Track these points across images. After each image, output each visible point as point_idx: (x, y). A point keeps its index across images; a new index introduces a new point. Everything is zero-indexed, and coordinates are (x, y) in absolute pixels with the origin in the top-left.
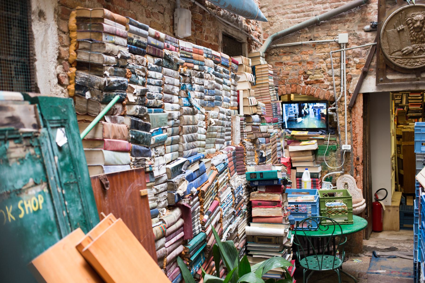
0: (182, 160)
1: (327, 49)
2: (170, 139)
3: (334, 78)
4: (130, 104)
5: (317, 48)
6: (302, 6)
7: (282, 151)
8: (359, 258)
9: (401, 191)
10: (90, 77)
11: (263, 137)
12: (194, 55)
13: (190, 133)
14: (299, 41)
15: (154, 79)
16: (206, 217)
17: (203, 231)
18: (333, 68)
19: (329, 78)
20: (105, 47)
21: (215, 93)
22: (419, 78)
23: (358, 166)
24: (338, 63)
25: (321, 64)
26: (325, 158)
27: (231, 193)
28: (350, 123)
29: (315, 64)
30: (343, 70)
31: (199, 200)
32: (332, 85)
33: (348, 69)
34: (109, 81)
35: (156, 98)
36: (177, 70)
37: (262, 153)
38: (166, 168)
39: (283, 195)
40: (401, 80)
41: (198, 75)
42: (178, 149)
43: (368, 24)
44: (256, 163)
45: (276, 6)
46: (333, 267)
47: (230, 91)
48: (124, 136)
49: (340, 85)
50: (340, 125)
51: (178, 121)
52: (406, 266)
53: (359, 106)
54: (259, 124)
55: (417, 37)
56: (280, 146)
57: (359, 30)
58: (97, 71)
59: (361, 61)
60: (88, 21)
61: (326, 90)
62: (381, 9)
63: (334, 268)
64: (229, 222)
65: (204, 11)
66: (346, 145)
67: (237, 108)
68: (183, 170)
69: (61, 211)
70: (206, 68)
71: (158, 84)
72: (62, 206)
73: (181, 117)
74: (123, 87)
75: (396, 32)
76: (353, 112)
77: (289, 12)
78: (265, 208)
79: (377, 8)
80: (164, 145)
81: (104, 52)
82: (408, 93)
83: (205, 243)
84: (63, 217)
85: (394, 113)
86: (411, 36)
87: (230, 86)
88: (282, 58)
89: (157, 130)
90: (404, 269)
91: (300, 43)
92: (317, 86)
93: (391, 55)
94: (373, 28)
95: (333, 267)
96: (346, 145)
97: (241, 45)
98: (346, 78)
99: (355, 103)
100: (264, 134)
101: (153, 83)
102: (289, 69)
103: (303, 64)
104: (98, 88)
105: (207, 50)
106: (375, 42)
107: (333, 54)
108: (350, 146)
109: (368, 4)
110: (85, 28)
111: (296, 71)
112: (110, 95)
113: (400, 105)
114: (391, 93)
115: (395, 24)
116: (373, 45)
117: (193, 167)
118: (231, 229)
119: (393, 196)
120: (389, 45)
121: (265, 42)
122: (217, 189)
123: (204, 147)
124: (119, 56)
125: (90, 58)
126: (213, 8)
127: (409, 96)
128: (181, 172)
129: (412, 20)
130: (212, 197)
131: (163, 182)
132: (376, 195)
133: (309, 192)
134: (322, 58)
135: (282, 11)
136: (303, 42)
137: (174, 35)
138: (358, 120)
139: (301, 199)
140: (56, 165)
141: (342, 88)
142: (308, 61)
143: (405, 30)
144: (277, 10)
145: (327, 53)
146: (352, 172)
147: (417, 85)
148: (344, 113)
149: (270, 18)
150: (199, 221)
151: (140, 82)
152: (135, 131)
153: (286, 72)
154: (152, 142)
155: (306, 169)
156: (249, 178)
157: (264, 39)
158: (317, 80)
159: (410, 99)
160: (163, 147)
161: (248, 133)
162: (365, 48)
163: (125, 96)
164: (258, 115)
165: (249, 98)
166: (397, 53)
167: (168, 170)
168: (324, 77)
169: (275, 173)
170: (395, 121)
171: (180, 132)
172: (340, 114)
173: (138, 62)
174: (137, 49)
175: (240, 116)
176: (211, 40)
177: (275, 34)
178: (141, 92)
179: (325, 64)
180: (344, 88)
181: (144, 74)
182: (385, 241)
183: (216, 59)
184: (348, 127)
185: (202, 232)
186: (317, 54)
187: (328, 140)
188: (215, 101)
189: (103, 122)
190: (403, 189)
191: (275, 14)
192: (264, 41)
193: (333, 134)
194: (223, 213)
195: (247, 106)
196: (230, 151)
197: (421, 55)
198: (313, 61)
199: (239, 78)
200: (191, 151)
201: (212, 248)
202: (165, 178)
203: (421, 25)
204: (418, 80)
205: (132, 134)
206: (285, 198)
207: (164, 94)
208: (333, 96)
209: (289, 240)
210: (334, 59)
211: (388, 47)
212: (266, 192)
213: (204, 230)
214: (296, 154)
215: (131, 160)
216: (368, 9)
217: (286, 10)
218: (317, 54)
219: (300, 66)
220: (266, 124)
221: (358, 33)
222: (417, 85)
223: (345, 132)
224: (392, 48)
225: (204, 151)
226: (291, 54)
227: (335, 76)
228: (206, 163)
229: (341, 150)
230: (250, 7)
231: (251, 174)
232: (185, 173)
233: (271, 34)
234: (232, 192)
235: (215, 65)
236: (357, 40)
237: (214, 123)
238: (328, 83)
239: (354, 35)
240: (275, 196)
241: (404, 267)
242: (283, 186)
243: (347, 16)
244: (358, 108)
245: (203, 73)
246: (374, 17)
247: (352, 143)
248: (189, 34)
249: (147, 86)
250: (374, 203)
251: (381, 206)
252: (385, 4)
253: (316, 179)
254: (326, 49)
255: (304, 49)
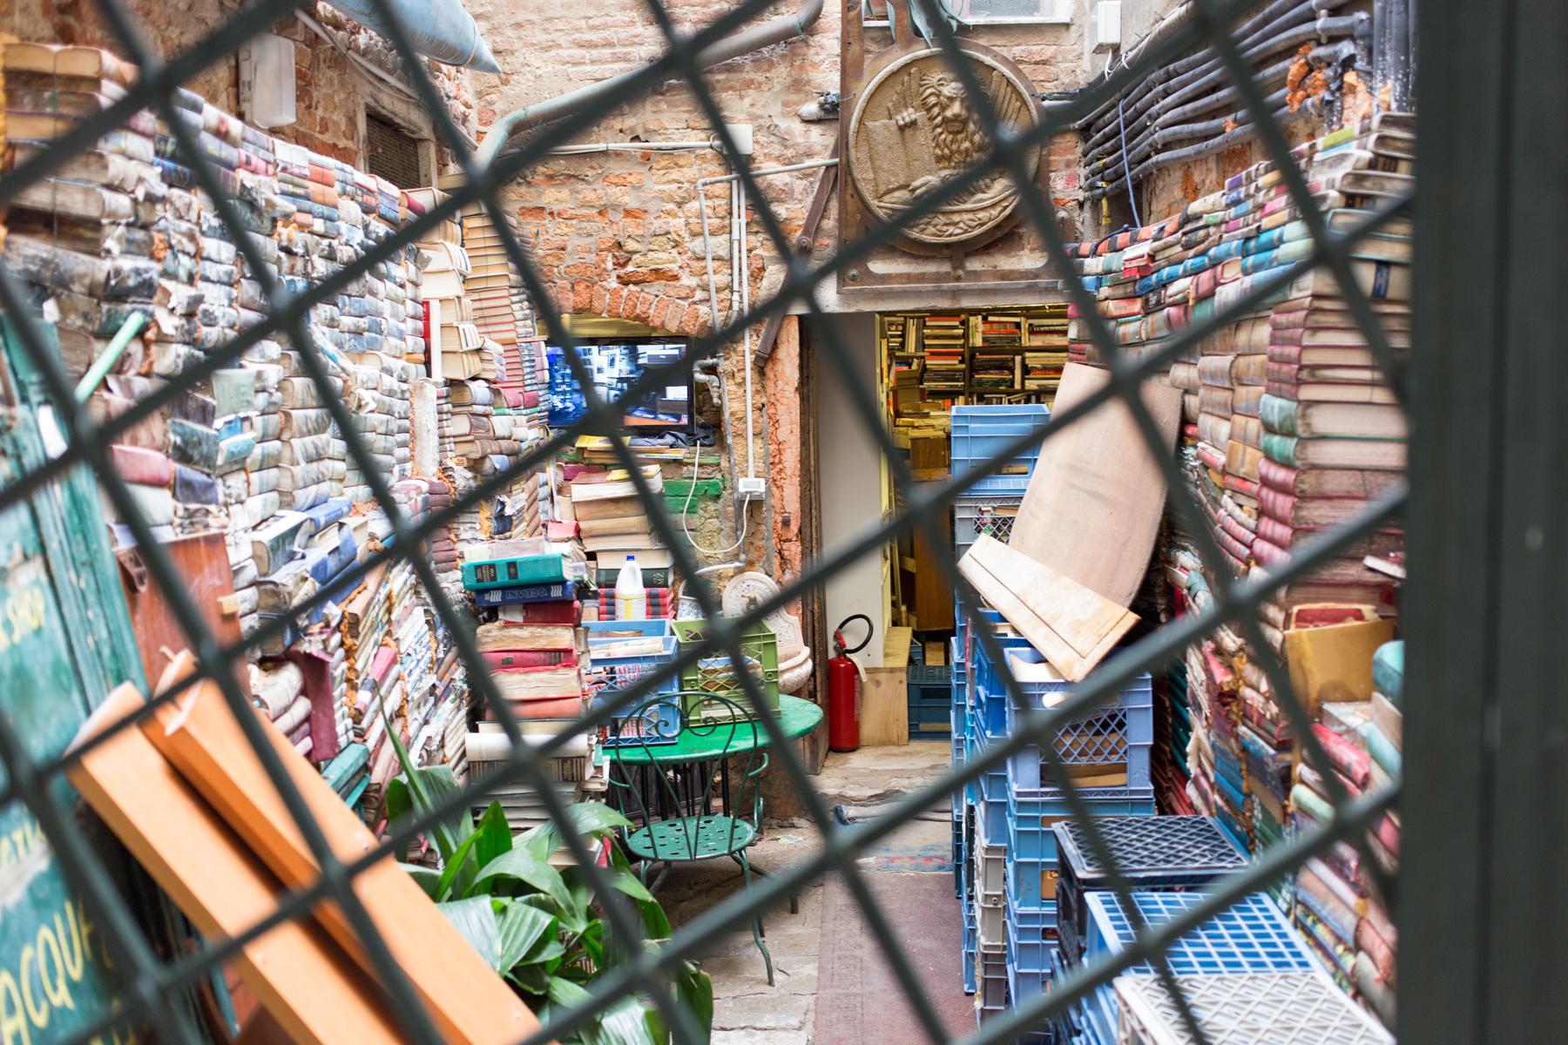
0: (291, 518)
1: (689, 173)
2: (258, 451)
3: (711, 265)
4: (163, 339)
5: (655, 166)
6: (605, 27)
7: (552, 501)
8: (794, 830)
9: (908, 625)
10: (56, 256)
11: (501, 453)
12: (313, 187)
13: (309, 433)
14: (598, 142)
15: (216, 262)
16: (363, 696)
17: (357, 739)
18: (707, 233)
19: (695, 264)
20: (105, 167)
21: (367, 307)
22: (960, 272)
23: (785, 546)
24: (723, 218)
25: (670, 219)
26: (687, 522)
27: (426, 627)
28: (761, 410)
29: (651, 218)
30: (740, 241)
31: (342, 644)
32: (705, 288)
33: (752, 238)
34: (118, 272)
35: (222, 323)
36: (270, 236)
37: (503, 504)
38: (253, 542)
39: (575, 632)
40: (908, 278)
41: (323, 250)
42: (278, 485)
43: (813, 99)
44: (483, 537)
45: (520, 18)
46: (730, 846)
47: (403, 303)
48: (154, 439)
49: (730, 287)
50: (732, 414)
51: (277, 396)
52: (932, 840)
53: (789, 354)
54: (489, 409)
55: (954, 147)
56: (546, 484)
57: (784, 115)
58: (80, 238)
59: (792, 215)
60: (46, 84)
61: (686, 303)
62: (849, 56)
63: (733, 848)
64: (423, 715)
65: (317, 36)
66: (751, 478)
67: (422, 357)
68: (296, 548)
69: (82, 637)
70: (343, 227)
71: (225, 279)
72: (82, 622)
73: (286, 384)
74: (147, 289)
75: (894, 128)
76: (770, 374)
77: (561, 41)
78: (526, 672)
79: (839, 51)
80: (244, 469)
81: (104, 181)
82: (923, 317)
83: (364, 776)
84: (87, 652)
85: (886, 380)
86: (937, 146)
87: (402, 286)
88: (540, 194)
89: (230, 422)
90: (925, 849)
91: (601, 146)
92: (657, 287)
93: (880, 198)
94: (825, 110)
95: (730, 846)
96: (751, 478)
97: (416, 147)
98: (749, 266)
99: (775, 345)
100: (503, 443)
101: (214, 277)
102: (567, 230)
103: (611, 215)
104: (83, 290)
105: (342, 170)
106: (835, 153)
107: (708, 187)
108: (762, 481)
109: (812, 35)
110: (36, 105)
111: (590, 240)
112: (117, 312)
113: (898, 354)
114: (877, 316)
115: (890, 105)
116: (828, 167)
117: (323, 539)
118: (429, 738)
119: (888, 638)
120: (875, 170)
121: (487, 137)
122: (389, 611)
123: (341, 480)
124: (140, 194)
125: (54, 199)
126: (338, 26)
127: (925, 326)
128: (291, 557)
129: (938, 96)
130: (376, 635)
131: (245, 584)
132: (837, 637)
133: (640, 630)
134: (671, 199)
135: (540, 37)
136: (612, 146)
137: (240, 116)
138: (785, 401)
139: (619, 649)
140: (60, 509)
141: (736, 297)
142: (627, 207)
143: (919, 123)
144: (523, 33)
145: (686, 185)
146: (770, 565)
147: (955, 294)
148: (744, 379)
149: (500, 59)
150: (345, 709)
151: (183, 274)
152: (181, 425)
153: (558, 241)
154: (220, 461)
155: (630, 558)
156: (472, 582)
157: (483, 129)
158: (657, 270)
159: (928, 337)
160: (243, 475)
161: (459, 440)
162: (806, 174)
163: (152, 315)
164: (486, 380)
165: (461, 327)
166: (897, 194)
167: (258, 547)
168: (680, 260)
169: (556, 561)
170: (888, 403)
171: (282, 430)
172: (731, 382)
173: (177, 210)
174: (176, 171)
175: (436, 384)
176: (335, 134)
177: (518, 113)
178: (189, 304)
179: (683, 220)
180: (741, 296)
181: (191, 248)
182: (868, 775)
183: (365, 197)
184: (755, 421)
185: (353, 742)
186: (657, 187)
187: (693, 464)
188: (366, 334)
189: (106, 395)
190: (913, 620)
191: (518, 45)
192: (480, 134)
193: (710, 446)
194: (409, 688)
195: (454, 353)
196: (413, 494)
197: (965, 202)
198: (644, 207)
199: (428, 260)
200: (313, 490)
201: (387, 792)
202: (251, 572)
203: (964, 113)
204: (958, 279)
205: (175, 432)
206: (583, 642)
207: (240, 310)
208: (709, 323)
209: (599, 769)
210: (710, 203)
211: (871, 175)
212: (528, 622)
213: (361, 735)
214: (594, 510)
215: (175, 512)
216: (812, 51)
217: (555, 36)
218: (657, 187)
219: (600, 222)
220: (507, 411)
221: (783, 124)
222: (955, 294)
223: (746, 439)
224: (883, 177)
225: (341, 494)
226: (573, 180)
227: (713, 259)
228: (355, 529)
229: (736, 495)
230: (455, 26)
231: (478, 567)
232: (303, 557)
233: (505, 113)
234: (427, 622)
235: (366, 217)
236: (778, 147)
237: (372, 406)
238: (694, 282)
239: (771, 130)
240: (556, 635)
241: (924, 843)
242: (577, 603)
243: (747, 68)
244: (786, 361)
245: (335, 243)
246: (829, 80)
247: (768, 473)
248: (287, 118)
249: (201, 284)
250: (831, 662)
251: (854, 669)
252: (862, 40)
253: (659, 590)
254: (684, 170)
255: (615, 168)
